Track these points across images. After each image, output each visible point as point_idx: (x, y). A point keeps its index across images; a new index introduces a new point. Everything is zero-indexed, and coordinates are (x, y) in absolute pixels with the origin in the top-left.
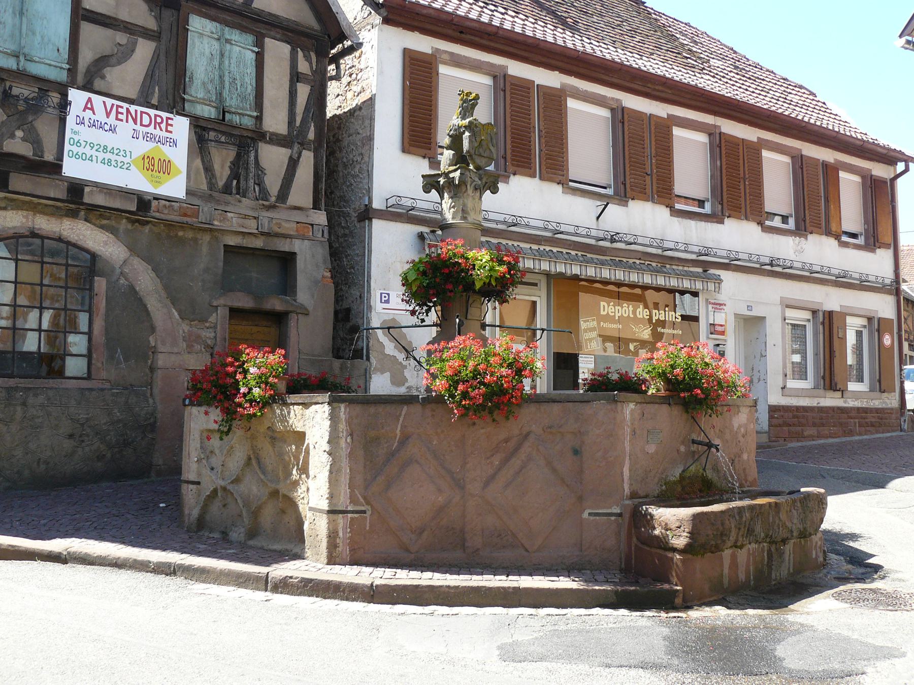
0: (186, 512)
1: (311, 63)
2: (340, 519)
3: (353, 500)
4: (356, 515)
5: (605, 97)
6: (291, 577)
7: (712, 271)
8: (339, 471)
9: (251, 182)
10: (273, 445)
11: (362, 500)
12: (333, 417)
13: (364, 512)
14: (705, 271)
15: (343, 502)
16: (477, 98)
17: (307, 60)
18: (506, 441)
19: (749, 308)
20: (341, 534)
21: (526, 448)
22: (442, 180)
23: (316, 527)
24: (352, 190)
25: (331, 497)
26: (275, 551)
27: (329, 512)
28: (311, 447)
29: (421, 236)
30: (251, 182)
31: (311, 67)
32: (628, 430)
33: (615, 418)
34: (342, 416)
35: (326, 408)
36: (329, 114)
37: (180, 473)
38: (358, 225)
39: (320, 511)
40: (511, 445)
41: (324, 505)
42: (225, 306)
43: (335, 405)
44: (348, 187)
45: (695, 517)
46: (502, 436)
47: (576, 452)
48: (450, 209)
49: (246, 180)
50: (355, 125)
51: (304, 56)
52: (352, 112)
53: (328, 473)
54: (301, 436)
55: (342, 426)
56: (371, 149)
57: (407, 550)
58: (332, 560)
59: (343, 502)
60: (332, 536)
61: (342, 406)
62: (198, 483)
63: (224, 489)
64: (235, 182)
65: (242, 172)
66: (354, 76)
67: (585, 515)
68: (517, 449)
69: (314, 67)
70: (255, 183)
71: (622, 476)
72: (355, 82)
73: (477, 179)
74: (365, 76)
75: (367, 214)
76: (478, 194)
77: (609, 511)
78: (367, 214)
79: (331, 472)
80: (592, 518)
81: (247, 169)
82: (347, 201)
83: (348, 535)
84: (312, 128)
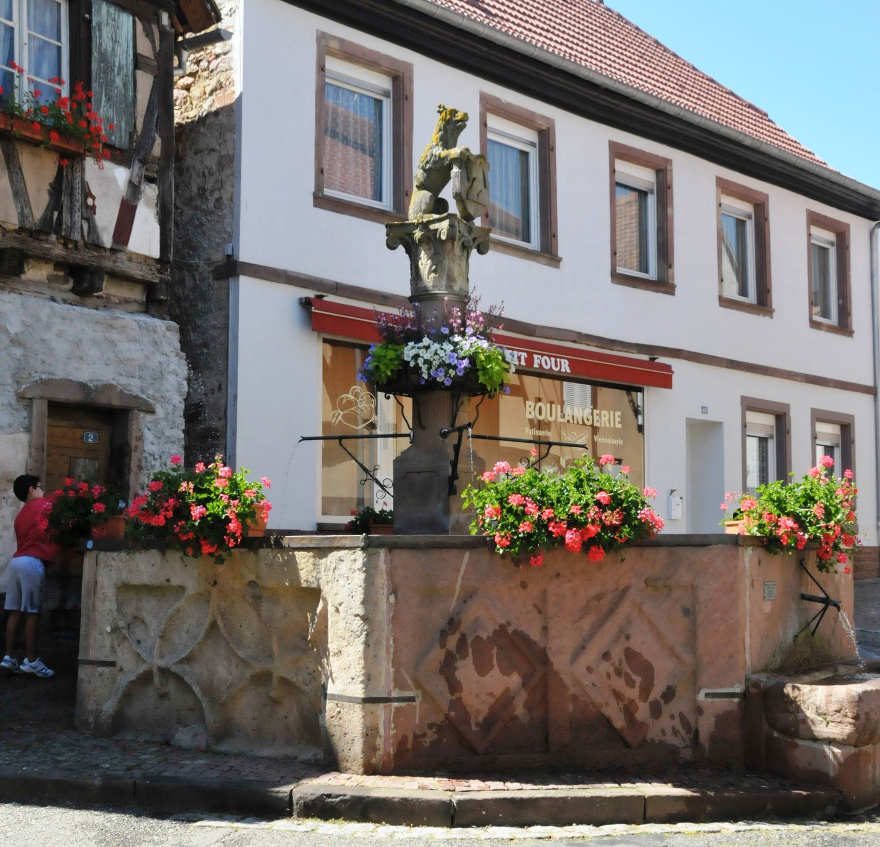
0: (91, 706)
1: (153, 42)
2: (380, 709)
3: (399, 683)
4: (403, 704)
5: (533, 114)
6: (329, 796)
7: (662, 360)
8: (378, 643)
9: (77, 217)
10: (257, 608)
11: (410, 682)
12: (369, 569)
13: (412, 699)
14: (653, 359)
15: (385, 686)
16: (465, 118)
17: (147, 35)
18: (599, 597)
19: (704, 410)
20: (382, 731)
21: (625, 608)
22: (418, 234)
23: (347, 723)
24: (204, 233)
25: (368, 679)
26: (267, 758)
27: (367, 700)
28: (331, 609)
29: (306, 304)
30: (77, 217)
31: (154, 48)
32: (748, 583)
33: (736, 568)
34: (382, 565)
35: (360, 556)
36: (177, 119)
37: (76, 652)
38: (216, 284)
39: (352, 700)
40: (606, 603)
41: (358, 691)
42: (42, 398)
43: (371, 550)
44: (196, 227)
45: (862, 698)
46: (593, 592)
47: (687, 612)
48: (429, 273)
49: (72, 213)
50: (209, 140)
51: (145, 30)
52: (202, 120)
53: (361, 648)
54: (315, 594)
55: (382, 580)
56: (236, 176)
57: (473, 751)
58: (370, 770)
59: (385, 686)
60: (370, 734)
61: (382, 553)
62: (113, 664)
63: (165, 672)
64: (56, 214)
65: (65, 199)
66: (204, 64)
67: (701, 697)
68: (612, 610)
69: (158, 48)
70: (83, 218)
71: (744, 643)
72: (206, 74)
73: (466, 234)
74: (223, 66)
75: (231, 268)
76: (465, 254)
77: (731, 690)
78: (231, 268)
79: (367, 644)
80: (709, 700)
81: (71, 195)
82: (194, 249)
83: (392, 732)
84: (158, 141)
